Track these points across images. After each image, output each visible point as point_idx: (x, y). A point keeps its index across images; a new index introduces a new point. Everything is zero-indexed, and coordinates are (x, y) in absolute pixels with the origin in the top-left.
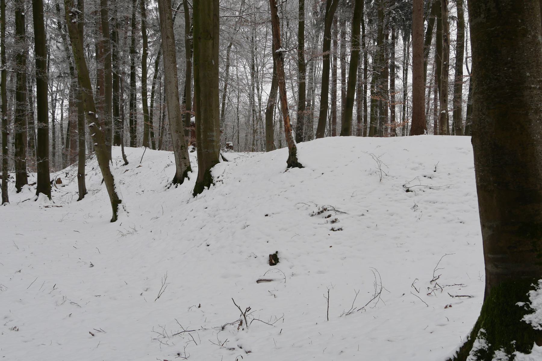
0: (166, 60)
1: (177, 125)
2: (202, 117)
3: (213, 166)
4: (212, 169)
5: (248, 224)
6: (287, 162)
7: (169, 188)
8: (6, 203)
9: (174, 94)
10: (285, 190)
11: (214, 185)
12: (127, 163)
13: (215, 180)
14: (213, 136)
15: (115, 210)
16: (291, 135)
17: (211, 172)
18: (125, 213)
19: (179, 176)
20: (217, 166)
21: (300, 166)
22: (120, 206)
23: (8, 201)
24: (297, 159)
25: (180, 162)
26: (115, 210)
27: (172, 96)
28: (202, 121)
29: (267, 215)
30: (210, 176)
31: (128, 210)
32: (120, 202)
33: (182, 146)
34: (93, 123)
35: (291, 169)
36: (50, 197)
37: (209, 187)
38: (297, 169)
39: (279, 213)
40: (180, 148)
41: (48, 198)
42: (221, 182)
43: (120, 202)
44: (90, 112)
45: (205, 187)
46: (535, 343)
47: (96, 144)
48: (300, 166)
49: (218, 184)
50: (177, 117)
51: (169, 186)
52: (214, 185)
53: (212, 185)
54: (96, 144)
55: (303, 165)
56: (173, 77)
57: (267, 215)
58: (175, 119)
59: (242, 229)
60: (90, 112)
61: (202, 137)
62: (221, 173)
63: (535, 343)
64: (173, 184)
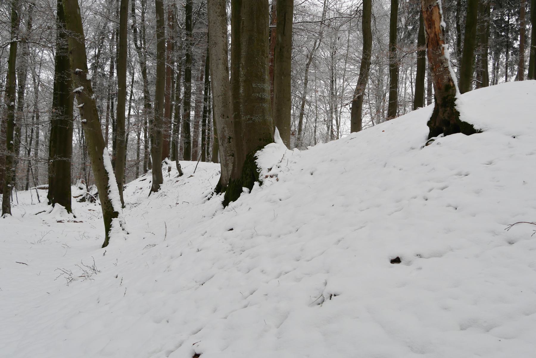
0: (211, 11)
1: (224, 106)
2: (243, 53)
3: (261, 147)
4: (258, 153)
5: (332, 288)
6: (429, 124)
7: (209, 199)
8: (6, 214)
9: (221, 62)
10: (442, 185)
11: (261, 183)
12: (181, 174)
13: (263, 173)
14: (264, 90)
15: (108, 227)
16: (442, 54)
17: (256, 158)
18: (123, 234)
19: (224, 181)
20: (269, 148)
21: (468, 129)
22: (115, 222)
23: (10, 213)
24: (458, 113)
25: (226, 161)
26: (108, 227)
27: (218, 65)
28: (243, 61)
29: (397, 260)
30: (255, 166)
31: (128, 229)
32: (116, 215)
33: (230, 138)
34: (82, 88)
35: (439, 139)
36: (69, 210)
37: (250, 187)
38: (459, 136)
39: (439, 255)
40: (226, 140)
41: (66, 211)
42: (274, 178)
43: (116, 215)
44: (77, 70)
45: (245, 189)
46: (224, 194)
47: (85, 120)
48: (468, 129)
49: (267, 182)
50: (225, 94)
51: (209, 196)
52: (261, 183)
53: (256, 184)
54: (85, 120)
55: (476, 127)
56: (221, 35)
57: (397, 260)
58: (221, 97)
59: (312, 304)
60: (77, 70)
61: (241, 91)
62: (276, 162)
63: (224, 194)
64: (215, 193)
